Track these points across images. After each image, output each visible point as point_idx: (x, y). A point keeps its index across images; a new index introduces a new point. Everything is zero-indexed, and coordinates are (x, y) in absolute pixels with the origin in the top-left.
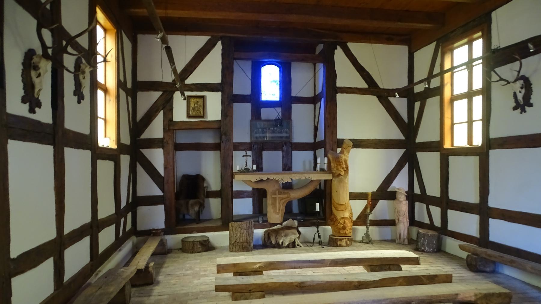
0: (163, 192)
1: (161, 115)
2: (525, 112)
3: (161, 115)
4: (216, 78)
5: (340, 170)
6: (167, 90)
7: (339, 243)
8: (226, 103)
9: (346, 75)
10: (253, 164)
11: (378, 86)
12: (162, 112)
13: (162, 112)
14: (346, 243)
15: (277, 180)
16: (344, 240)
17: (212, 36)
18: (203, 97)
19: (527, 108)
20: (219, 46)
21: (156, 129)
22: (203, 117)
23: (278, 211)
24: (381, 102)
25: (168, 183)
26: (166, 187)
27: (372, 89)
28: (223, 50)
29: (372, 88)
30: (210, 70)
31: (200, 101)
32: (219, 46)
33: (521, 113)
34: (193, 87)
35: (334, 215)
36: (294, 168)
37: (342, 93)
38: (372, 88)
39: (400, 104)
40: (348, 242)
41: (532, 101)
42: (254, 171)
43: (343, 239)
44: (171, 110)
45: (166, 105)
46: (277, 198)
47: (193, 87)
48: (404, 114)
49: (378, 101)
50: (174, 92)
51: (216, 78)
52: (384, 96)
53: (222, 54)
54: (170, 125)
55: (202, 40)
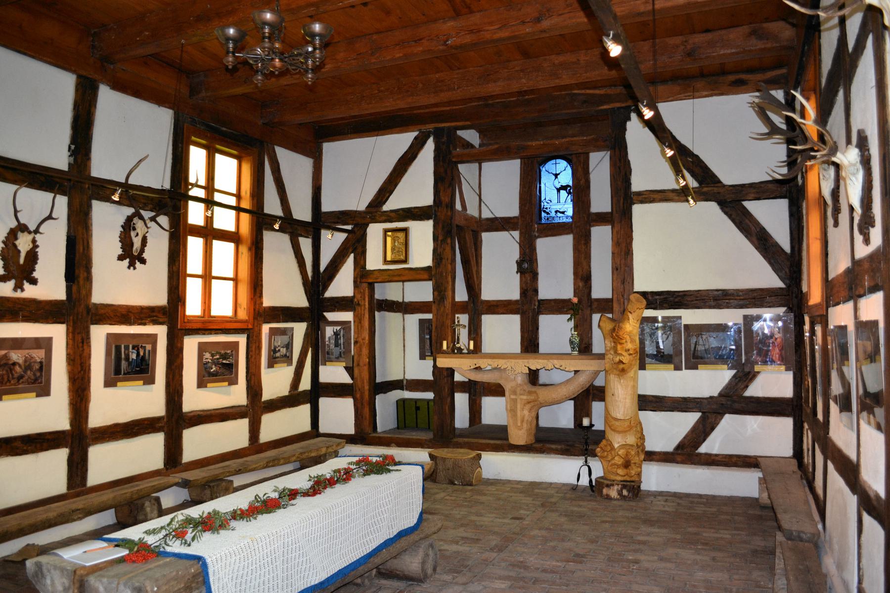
0: (352, 379)
1: (350, 261)
2: (135, 268)
3: (350, 261)
4: (425, 197)
5: (621, 355)
6: (355, 224)
7: (605, 491)
8: (440, 238)
9: (649, 166)
10: (470, 339)
11: (719, 182)
12: (352, 255)
13: (352, 255)
14: (620, 493)
15: (505, 369)
16: (616, 487)
17: (420, 130)
18: (405, 230)
19: (138, 264)
20: (430, 146)
21: (343, 285)
22: (405, 261)
23: (519, 424)
24: (726, 213)
25: (358, 365)
26: (356, 371)
27: (705, 189)
28: (435, 150)
29: (706, 184)
30: (417, 187)
31: (401, 235)
32: (430, 146)
33: (129, 268)
34: (393, 215)
35: (608, 440)
36: (542, 349)
37: (642, 202)
38: (706, 184)
39: (772, 215)
40: (625, 492)
41: (145, 255)
42: (470, 352)
43: (613, 485)
44: (364, 252)
45: (356, 245)
46: (519, 401)
47: (393, 215)
48: (782, 237)
49: (720, 211)
50: (367, 225)
51: (425, 197)
52: (733, 201)
53: (435, 158)
54: (363, 276)
55: (403, 140)
